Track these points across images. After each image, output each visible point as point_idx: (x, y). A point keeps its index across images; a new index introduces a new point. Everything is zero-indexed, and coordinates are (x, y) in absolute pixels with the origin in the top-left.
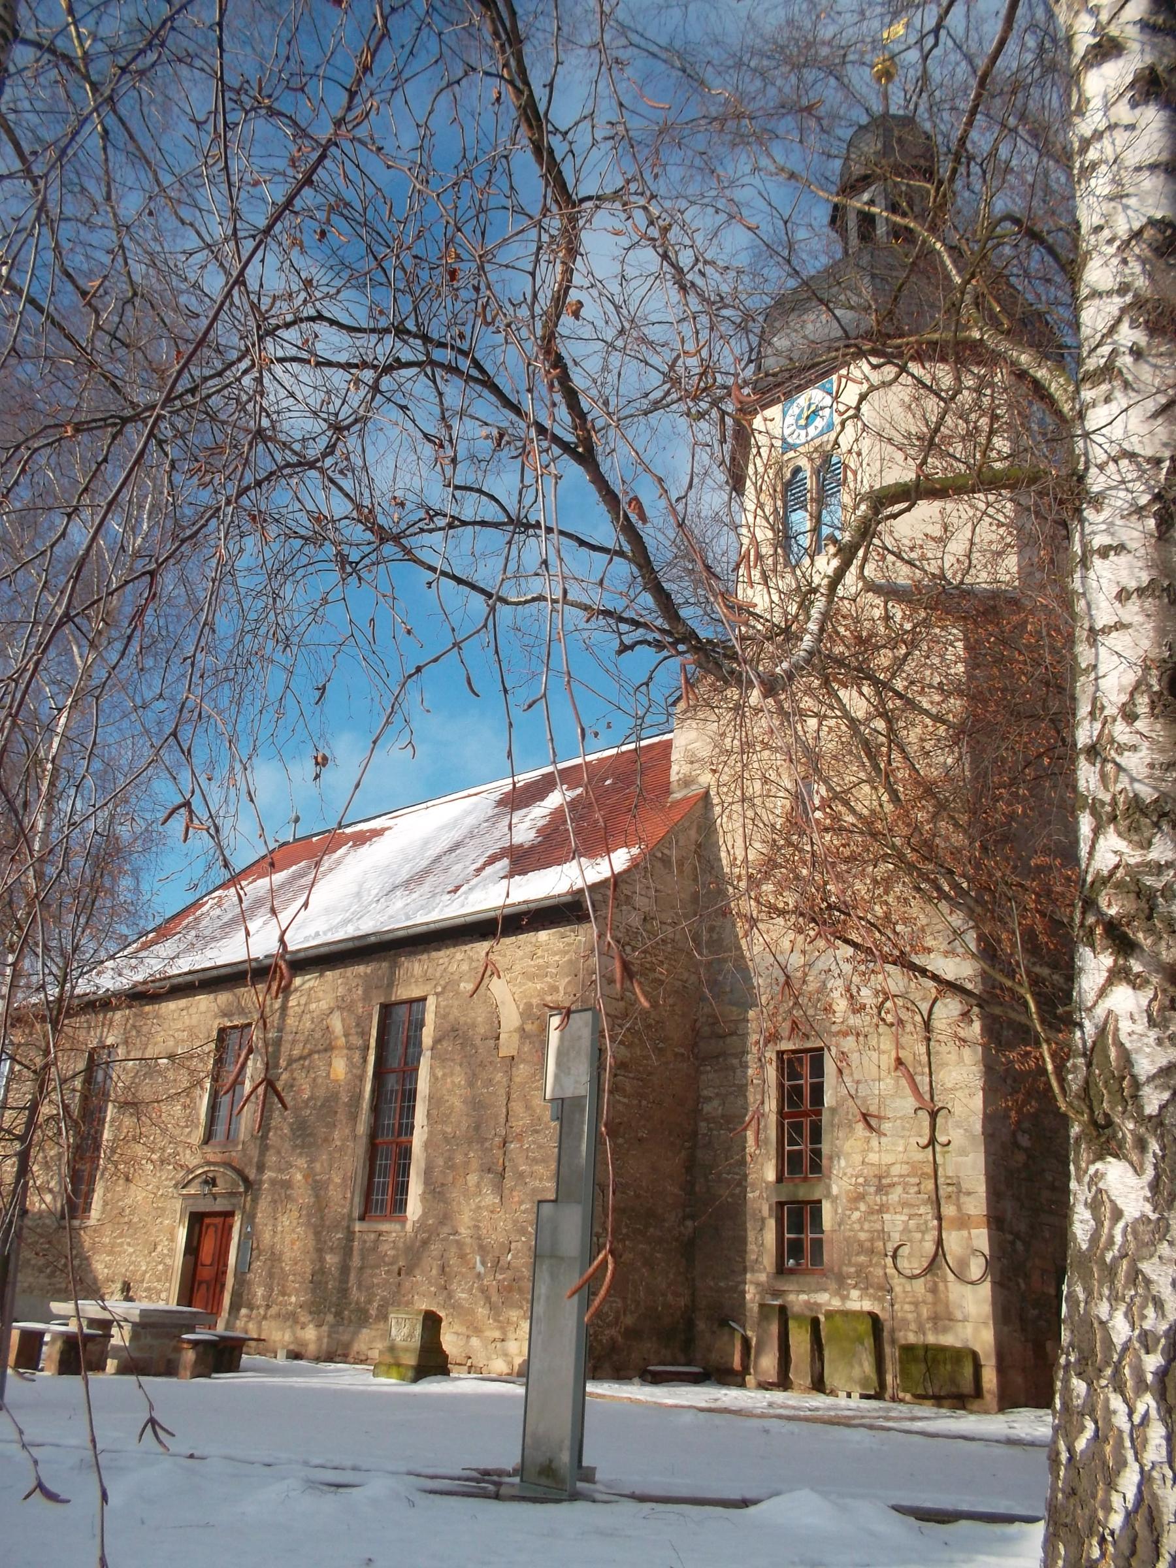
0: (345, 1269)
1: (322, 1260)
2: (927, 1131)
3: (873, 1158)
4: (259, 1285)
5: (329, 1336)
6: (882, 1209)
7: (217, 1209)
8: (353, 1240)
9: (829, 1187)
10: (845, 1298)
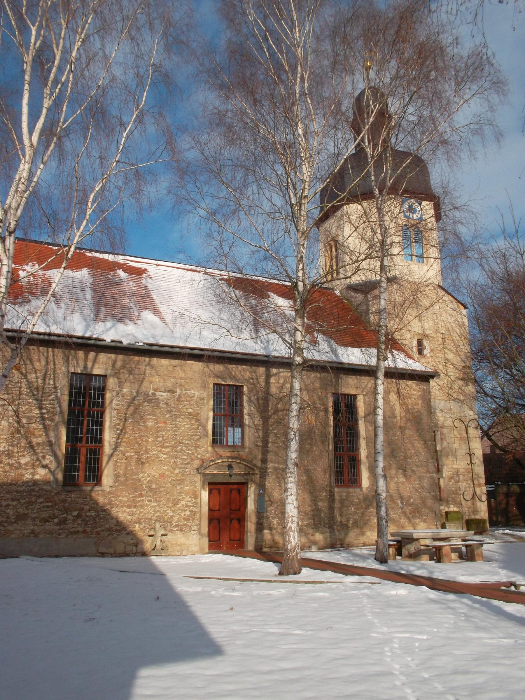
0: (331, 508)
1: (316, 505)
2: (469, 459)
3: (455, 466)
4: (274, 518)
5: (330, 537)
6: (459, 481)
7: (233, 481)
8: (334, 495)
9: (442, 475)
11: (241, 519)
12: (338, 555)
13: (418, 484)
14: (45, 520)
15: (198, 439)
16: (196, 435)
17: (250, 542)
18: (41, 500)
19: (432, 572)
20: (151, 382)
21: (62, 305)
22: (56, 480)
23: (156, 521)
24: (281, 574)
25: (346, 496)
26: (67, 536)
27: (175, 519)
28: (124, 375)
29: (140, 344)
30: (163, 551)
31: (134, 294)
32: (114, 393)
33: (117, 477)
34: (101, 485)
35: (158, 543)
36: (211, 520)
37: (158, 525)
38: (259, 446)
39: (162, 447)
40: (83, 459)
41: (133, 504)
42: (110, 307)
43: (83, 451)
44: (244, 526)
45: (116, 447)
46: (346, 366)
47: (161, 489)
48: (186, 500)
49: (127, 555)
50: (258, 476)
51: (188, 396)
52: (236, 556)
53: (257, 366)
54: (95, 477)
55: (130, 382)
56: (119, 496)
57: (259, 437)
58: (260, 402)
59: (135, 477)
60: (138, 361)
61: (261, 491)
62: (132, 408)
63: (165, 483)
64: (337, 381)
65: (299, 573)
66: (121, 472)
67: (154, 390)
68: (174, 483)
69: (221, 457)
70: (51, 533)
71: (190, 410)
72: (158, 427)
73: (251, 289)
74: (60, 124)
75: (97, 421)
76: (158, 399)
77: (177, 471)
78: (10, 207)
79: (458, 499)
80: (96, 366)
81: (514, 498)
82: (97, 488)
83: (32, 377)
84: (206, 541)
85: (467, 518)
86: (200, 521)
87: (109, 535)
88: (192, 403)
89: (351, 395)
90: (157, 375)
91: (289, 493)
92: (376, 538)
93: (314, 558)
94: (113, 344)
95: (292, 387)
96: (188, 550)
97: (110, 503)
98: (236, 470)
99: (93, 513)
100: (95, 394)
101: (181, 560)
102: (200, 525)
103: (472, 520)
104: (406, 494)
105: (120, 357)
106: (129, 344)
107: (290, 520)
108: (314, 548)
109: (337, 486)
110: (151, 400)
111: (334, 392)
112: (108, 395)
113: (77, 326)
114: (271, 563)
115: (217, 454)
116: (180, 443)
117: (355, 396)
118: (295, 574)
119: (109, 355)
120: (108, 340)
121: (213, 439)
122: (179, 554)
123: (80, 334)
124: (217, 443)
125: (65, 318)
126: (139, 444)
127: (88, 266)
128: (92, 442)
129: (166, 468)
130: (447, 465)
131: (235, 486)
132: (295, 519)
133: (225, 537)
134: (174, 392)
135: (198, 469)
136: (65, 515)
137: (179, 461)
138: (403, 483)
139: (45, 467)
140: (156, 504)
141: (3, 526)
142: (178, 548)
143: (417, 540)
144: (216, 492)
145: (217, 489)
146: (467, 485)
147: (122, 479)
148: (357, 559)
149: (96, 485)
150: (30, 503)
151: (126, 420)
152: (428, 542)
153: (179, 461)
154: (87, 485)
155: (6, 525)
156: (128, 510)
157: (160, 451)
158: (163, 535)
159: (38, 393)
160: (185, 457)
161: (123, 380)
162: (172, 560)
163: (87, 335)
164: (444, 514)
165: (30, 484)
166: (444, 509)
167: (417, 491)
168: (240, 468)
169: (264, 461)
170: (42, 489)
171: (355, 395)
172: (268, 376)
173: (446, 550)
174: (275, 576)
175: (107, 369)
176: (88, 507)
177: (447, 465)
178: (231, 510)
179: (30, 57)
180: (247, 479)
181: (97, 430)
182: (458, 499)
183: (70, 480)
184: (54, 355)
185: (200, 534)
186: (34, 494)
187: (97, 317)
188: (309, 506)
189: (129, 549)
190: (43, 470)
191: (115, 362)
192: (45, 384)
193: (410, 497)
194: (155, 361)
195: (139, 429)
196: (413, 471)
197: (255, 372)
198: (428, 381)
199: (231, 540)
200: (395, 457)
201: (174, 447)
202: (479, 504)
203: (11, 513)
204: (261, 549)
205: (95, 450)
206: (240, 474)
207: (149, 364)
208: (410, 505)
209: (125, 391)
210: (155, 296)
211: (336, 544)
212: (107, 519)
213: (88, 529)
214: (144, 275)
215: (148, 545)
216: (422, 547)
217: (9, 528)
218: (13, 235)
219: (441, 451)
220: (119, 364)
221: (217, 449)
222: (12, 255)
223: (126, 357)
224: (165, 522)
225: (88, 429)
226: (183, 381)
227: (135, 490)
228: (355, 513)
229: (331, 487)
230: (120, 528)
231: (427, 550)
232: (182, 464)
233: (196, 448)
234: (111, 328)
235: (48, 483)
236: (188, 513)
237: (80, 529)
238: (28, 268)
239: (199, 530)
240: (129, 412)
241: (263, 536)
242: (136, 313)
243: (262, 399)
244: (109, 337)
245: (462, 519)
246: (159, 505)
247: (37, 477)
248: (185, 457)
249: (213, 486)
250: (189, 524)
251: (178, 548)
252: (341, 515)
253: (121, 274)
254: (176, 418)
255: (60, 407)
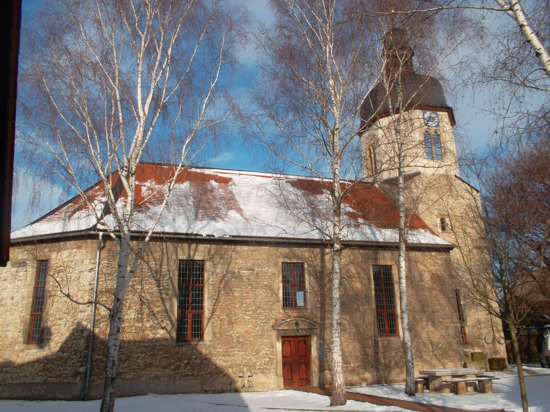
0: (376, 353)
3: (477, 317)
6: (481, 328)
7: (299, 335)
8: (378, 343)
9: (466, 324)
10: (474, 349)
11: (308, 363)
12: (379, 389)
13: (445, 332)
14: (165, 367)
15: (272, 304)
16: (270, 301)
17: (315, 380)
18: (162, 352)
19: (445, 402)
20: (236, 264)
21: (172, 210)
22: (172, 337)
23: (244, 366)
24: (331, 405)
25: (388, 343)
26: (180, 378)
27: (258, 364)
28: (217, 259)
29: (228, 236)
30: (250, 388)
31: (222, 198)
32: (210, 273)
33: (214, 334)
34: (203, 341)
35: (246, 382)
36: (284, 364)
37: (245, 369)
38: (318, 307)
39: (246, 311)
40: (189, 323)
41: (226, 354)
42: (205, 209)
43: (190, 316)
44: (310, 368)
45: (213, 312)
46: (382, 244)
47: (246, 342)
48: (266, 350)
49: (223, 391)
50: (318, 330)
51: (264, 272)
52: (303, 391)
53: (314, 247)
54: (199, 334)
55: (221, 264)
56: (216, 348)
57: (318, 301)
58: (318, 274)
59: (227, 334)
60: (227, 249)
61: (321, 342)
62: (223, 283)
63: (250, 338)
64: (376, 256)
65: (345, 404)
66: (217, 330)
67: (239, 269)
68: (256, 337)
69: (289, 317)
70: (169, 376)
71: (266, 283)
72: (243, 296)
73: (310, 188)
74: (162, 100)
75: (199, 294)
76: (242, 276)
77: (258, 328)
78: (131, 157)
79: (481, 343)
80: (197, 253)
81: (534, 339)
82: (200, 343)
83: (153, 264)
84: (281, 380)
85: (489, 357)
86: (276, 365)
87: (210, 377)
88: (266, 277)
89: (387, 266)
90: (241, 258)
91: (334, 345)
92: (405, 377)
93: (361, 392)
94: (208, 238)
95: (333, 267)
96: (268, 387)
97: (210, 353)
98: (302, 326)
99: (198, 361)
100: (196, 274)
101: (262, 395)
102: (276, 368)
103: (494, 359)
104: (435, 341)
105: (214, 246)
106: (219, 237)
107: (336, 364)
108: (364, 384)
109: (381, 336)
110: (236, 276)
111: (373, 264)
112: (206, 275)
113: (181, 226)
114: (327, 397)
115: (287, 315)
116: (259, 307)
117: (390, 266)
118: (342, 405)
119: (206, 245)
120: (205, 235)
121: (284, 304)
122: (262, 390)
123: (184, 231)
124: (286, 306)
125: (174, 220)
126: (230, 310)
127: (189, 180)
128: (196, 309)
129: (250, 326)
130: (470, 316)
131: (302, 338)
132: (340, 364)
133: (296, 377)
134: (253, 270)
135: (273, 327)
136: (178, 363)
137: (259, 321)
138: (433, 332)
139: (163, 328)
140: (243, 353)
141: (136, 372)
142: (261, 386)
143: (440, 377)
144: (287, 343)
145: (288, 341)
146: (488, 331)
147: (218, 335)
148: (393, 392)
149: (200, 340)
150: (155, 355)
151: (219, 292)
152: (449, 379)
153: (259, 321)
154: (194, 341)
155: (138, 371)
156: (223, 358)
157: (245, 314)
158: (249, 376)
159: (157, 276)
160: (263, 318)
161: (216, 263)
162: (255, 395)
163: (190, 232)
164: (470, 355)
165: (154, 341)
166: (469, 350)
167: (444, 337)
168: (305, 325)
169: (323, 319)
170: (162, 345)
171: (391, 266)
172: (323, 255)
173: (462, 385)
174: (327, 406)
175: (204, 256)
176: (195, 357)
177: (470, 316)
178: (299, 356)
179: (142, 55)
180: (310, 333)
181: (199, 300)
182: (481, 343)
183: (181, 338)
184: (166, 248)
185: (277, 375)
186: (156, 348)
187: (196, 218)
188: (359, 351)
189: (225, 387)
190: (162, 331)
191: (210, 250)
192: (161, 268)
193: (439, 343)
194: (238, 248)
195: (229, 298)
196: (440, 322)
197: (313, 252)
198: (449, 252)
199: (300, 379)
200: (425, 312)
201: (255, 311)
202: (498, 346)
203: (141, 362)
204: (324, 385)
205: (198, 315)
206: (304, 329)
207: (234, 250)
208: (439, 349)
209: (218, 271)
210: (238, 199)
211: (381, 381)
212: (209, 365)
213: (195, 373)
214: (230, 183)
215: (239, 384)
216: (444, 383)
217: (140, 373)
218: (134, 176)
219: (465, 305)
220: (213, 251)
221: (286, 311)
222: (134, 189)
223: (218, 246)
224: (250, 366)
225: (193, 300)
226: (259, 261)
227: (228, 343)
228: (395, 356)
229: (375, 336)
230: (219, 372)
231: (448, 384)
232: (261, 323)
233: (271, 310)
234: (206, 225)
235: (166, 340)
236: (267, 359)
237: (190, 373)
238: (148, 184)
239: (276, 372)
240: (221, 286)
241: (324, 375)
242: (224, 213)
243: (319, 272)
244: (204, 233)
245: (485, 358)
246: (245, 354)
247: (158, 336)
248: (263, 318)
249: (285, 339)
250: (268, 367)
251: (261, 386)
252: (384, 358)
253: (213, 182)
254: (256, 289)
255: (173, 284)
